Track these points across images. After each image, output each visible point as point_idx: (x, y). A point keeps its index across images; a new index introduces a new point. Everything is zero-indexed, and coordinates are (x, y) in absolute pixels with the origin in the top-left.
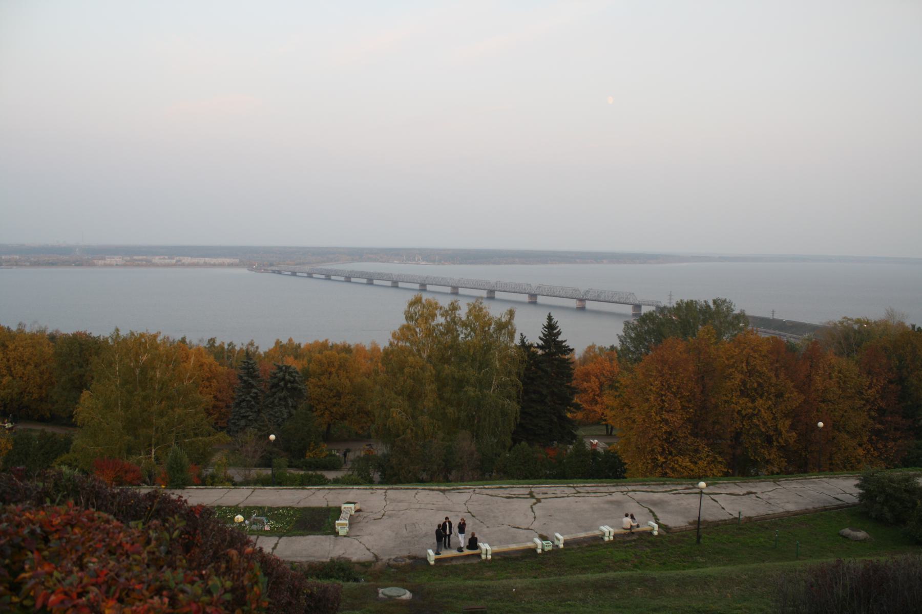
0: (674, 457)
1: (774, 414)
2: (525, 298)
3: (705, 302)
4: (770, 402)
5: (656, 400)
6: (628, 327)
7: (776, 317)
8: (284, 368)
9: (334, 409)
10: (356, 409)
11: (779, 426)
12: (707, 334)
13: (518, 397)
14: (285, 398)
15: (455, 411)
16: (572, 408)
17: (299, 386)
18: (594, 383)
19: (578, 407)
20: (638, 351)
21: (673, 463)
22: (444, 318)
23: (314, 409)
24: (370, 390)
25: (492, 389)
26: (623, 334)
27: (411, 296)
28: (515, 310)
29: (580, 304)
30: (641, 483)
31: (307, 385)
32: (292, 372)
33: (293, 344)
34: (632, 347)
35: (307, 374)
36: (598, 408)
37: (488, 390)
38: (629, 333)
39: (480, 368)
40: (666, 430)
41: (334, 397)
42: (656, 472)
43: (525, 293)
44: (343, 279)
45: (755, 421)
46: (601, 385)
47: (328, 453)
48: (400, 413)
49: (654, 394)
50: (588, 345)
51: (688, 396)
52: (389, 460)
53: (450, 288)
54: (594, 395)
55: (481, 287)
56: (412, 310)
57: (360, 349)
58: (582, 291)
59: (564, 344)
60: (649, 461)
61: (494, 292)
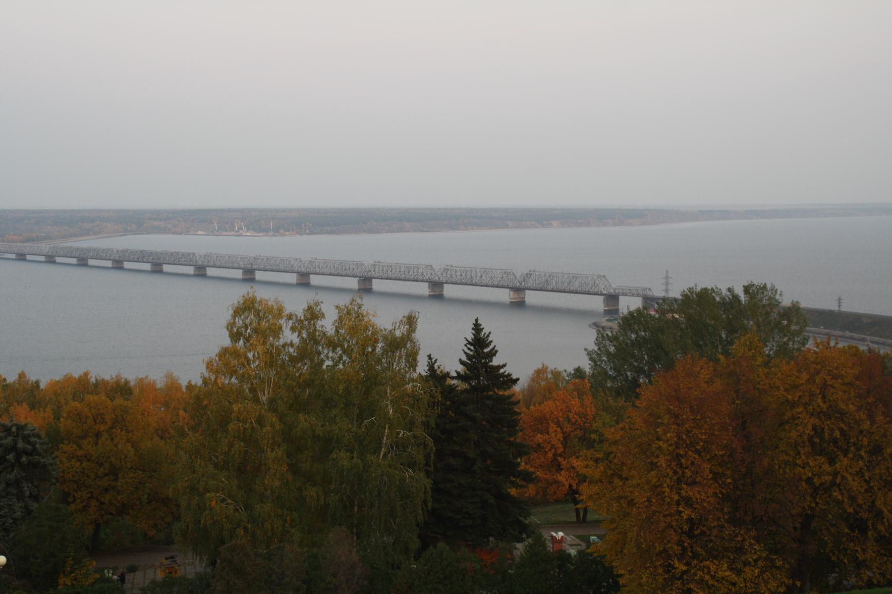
0: (701, 562)
1: (868, 482)
2: (424, 289)
3: (729, 290)
4: (861, 463)
5: (670, 465)
6: (603, 336)
7: (845, 308)
8: (14, 429)
9: (107, 497)
10: (146, 496)
11: (878, 503)
12: (750, 350)
13: (427, 464)
14: (17, 482)
15: (320, 493)
16: (518, 480)
17: (42, 460)
18: (555, 437)
19: (528, 477)
20: (622, 375)
21: (700, 573)
22: (296, 334)
23: (70, 499)
24: (169, 461)
25: (382, 454)
26: (596, 348)
27: (237, 294)
28: (417, 316)
29: (516, 296)
30: (133, 233)
31: (57, 457)
32: (29, 436)
33: (27, 383)
34: (611, 369)
35: (55, 438)
36: (562, 477)
37: (374, 453)
38: (605, 346)
39: (361, 417)
40: (690, 516)
41: (106, 475)
42: (671, 589)
43: (423, 281)
44: (109, 264)
45: (835, 494)
46: (566, 438)
47: (98, 576)
48: (223, 500)
49: (664, 455)
50: (535, 368)
51: (722, 456)
52: (208, 585)
53: (295, 275)
54: (555, 455)
55: (349, 272)
56: (239, 322)
57: (146, 387)
58: (518, 275)
59: (502, 371)
60: (660, 571)
61: (371, 281)
